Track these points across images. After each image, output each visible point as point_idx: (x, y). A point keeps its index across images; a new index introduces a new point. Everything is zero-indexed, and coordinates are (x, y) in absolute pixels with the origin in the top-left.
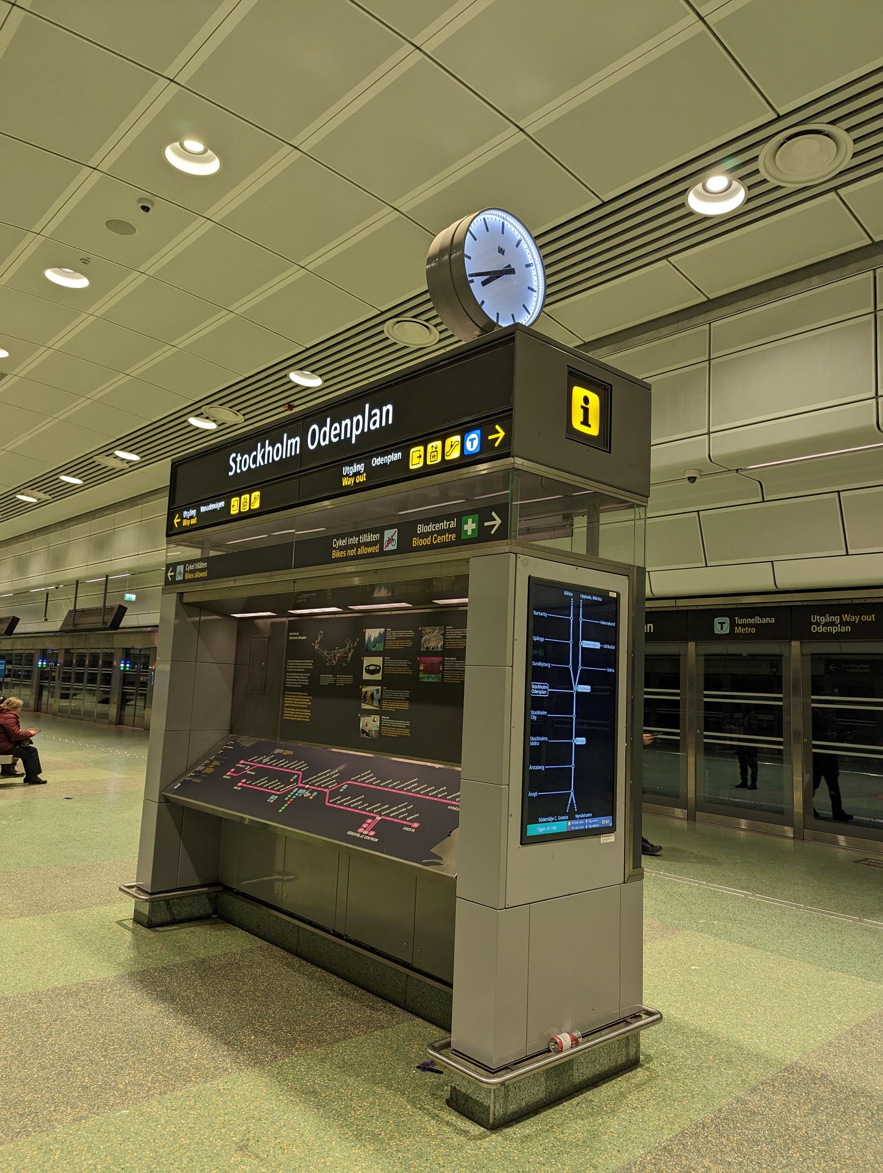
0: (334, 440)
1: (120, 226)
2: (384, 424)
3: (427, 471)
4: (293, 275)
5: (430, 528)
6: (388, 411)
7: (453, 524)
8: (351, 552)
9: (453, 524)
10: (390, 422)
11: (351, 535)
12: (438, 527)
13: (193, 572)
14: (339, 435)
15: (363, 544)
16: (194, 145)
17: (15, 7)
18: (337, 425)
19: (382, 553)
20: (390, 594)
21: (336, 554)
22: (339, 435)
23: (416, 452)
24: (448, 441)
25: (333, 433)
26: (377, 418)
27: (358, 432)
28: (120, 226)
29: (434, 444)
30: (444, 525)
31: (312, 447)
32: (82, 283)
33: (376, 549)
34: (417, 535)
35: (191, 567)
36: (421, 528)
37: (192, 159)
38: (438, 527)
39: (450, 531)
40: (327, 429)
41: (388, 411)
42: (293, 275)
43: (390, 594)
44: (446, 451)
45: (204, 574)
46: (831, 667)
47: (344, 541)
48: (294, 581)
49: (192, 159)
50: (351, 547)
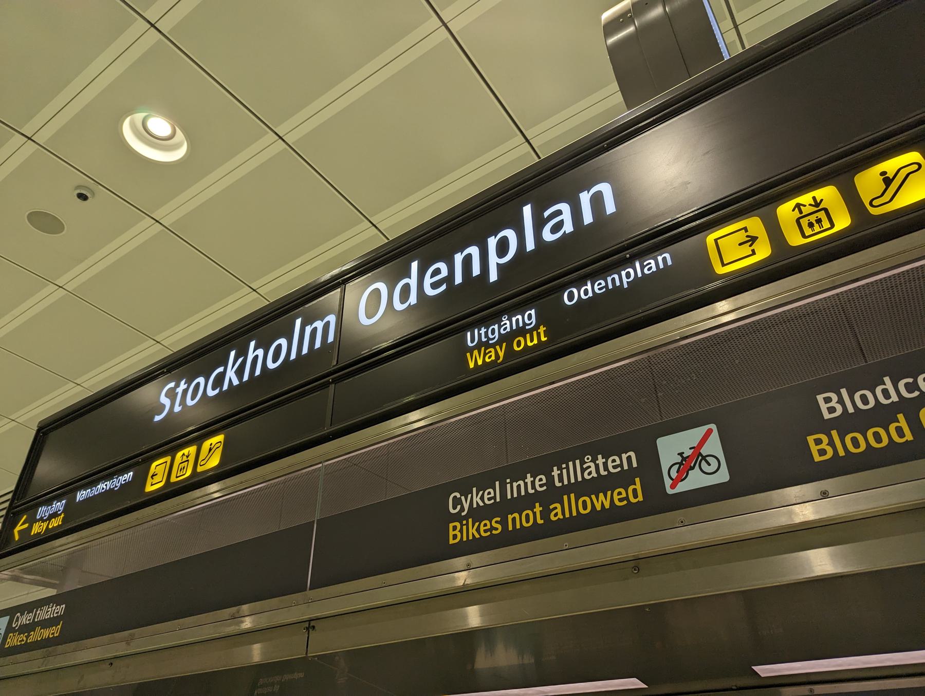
1: (45, 222)
3: (172, 491)
4: (48, 296)
8: (520, 520)
11: (484, 482)
13: (26, 629)
15: (568, 489)
16: (160, 126)
17: (152, 29)
19: (659, 503)
20: (529, 660)
21: (455, 534)
22: (621, 465)
23: (158, 467)
24: (207, 444)
28: (45, 222)
29: (186, 451)
33: (635, 493)
34: (825, 427)
35: (25, 619)
37: (154, 136)
39: (623, 479)
42: (48, 296)
43: (529, 660)
44: (201, 457)
45: (54, 632)
47: (488, 493)
48: (310, 625)
49: (154, 136)
50: (524, 502)
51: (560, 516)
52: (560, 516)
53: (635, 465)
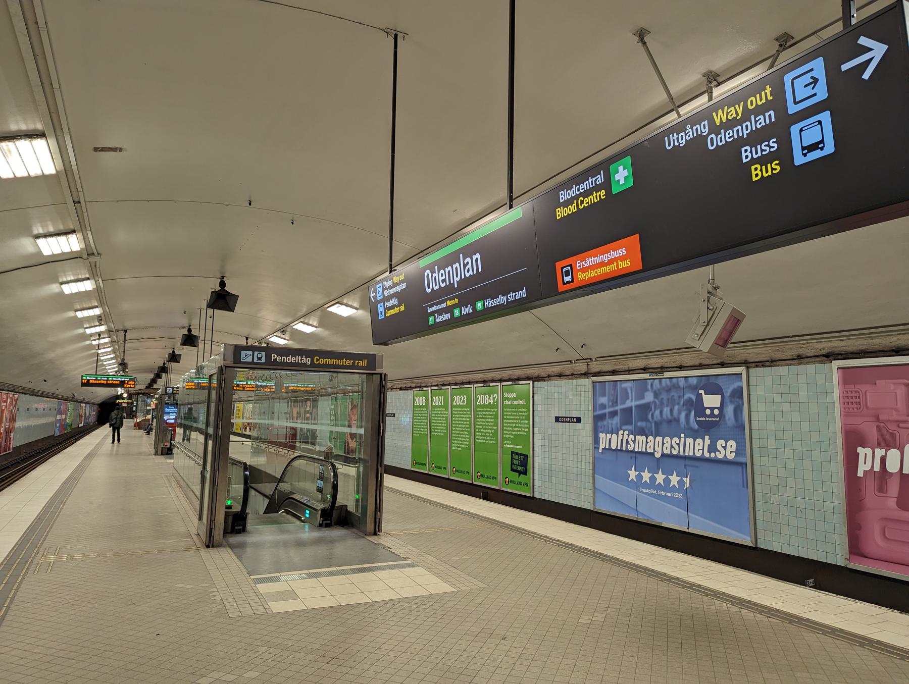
0: (728, 140)
2: (768, 122)
5: (574, 191)
6: (477, 259)
7: (600, 179)
9: (600, 179)
10: (773, 120)
12: (583, 187)
14: (444, 281)
18: (468, 260)
22: (733, 136)
25: (441, 278)
26: (469, 266)
27: (458, 279)
30: (589, 183)
31: (711, 148)
32: (845, 67)
36: (564, 196)
38: (583, 187)
40: (435, 275)
41: (477, 259)
46: (878, 50)
51: (763, 124)
52: (763, 124)
53: (773, 120)
